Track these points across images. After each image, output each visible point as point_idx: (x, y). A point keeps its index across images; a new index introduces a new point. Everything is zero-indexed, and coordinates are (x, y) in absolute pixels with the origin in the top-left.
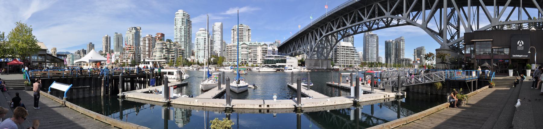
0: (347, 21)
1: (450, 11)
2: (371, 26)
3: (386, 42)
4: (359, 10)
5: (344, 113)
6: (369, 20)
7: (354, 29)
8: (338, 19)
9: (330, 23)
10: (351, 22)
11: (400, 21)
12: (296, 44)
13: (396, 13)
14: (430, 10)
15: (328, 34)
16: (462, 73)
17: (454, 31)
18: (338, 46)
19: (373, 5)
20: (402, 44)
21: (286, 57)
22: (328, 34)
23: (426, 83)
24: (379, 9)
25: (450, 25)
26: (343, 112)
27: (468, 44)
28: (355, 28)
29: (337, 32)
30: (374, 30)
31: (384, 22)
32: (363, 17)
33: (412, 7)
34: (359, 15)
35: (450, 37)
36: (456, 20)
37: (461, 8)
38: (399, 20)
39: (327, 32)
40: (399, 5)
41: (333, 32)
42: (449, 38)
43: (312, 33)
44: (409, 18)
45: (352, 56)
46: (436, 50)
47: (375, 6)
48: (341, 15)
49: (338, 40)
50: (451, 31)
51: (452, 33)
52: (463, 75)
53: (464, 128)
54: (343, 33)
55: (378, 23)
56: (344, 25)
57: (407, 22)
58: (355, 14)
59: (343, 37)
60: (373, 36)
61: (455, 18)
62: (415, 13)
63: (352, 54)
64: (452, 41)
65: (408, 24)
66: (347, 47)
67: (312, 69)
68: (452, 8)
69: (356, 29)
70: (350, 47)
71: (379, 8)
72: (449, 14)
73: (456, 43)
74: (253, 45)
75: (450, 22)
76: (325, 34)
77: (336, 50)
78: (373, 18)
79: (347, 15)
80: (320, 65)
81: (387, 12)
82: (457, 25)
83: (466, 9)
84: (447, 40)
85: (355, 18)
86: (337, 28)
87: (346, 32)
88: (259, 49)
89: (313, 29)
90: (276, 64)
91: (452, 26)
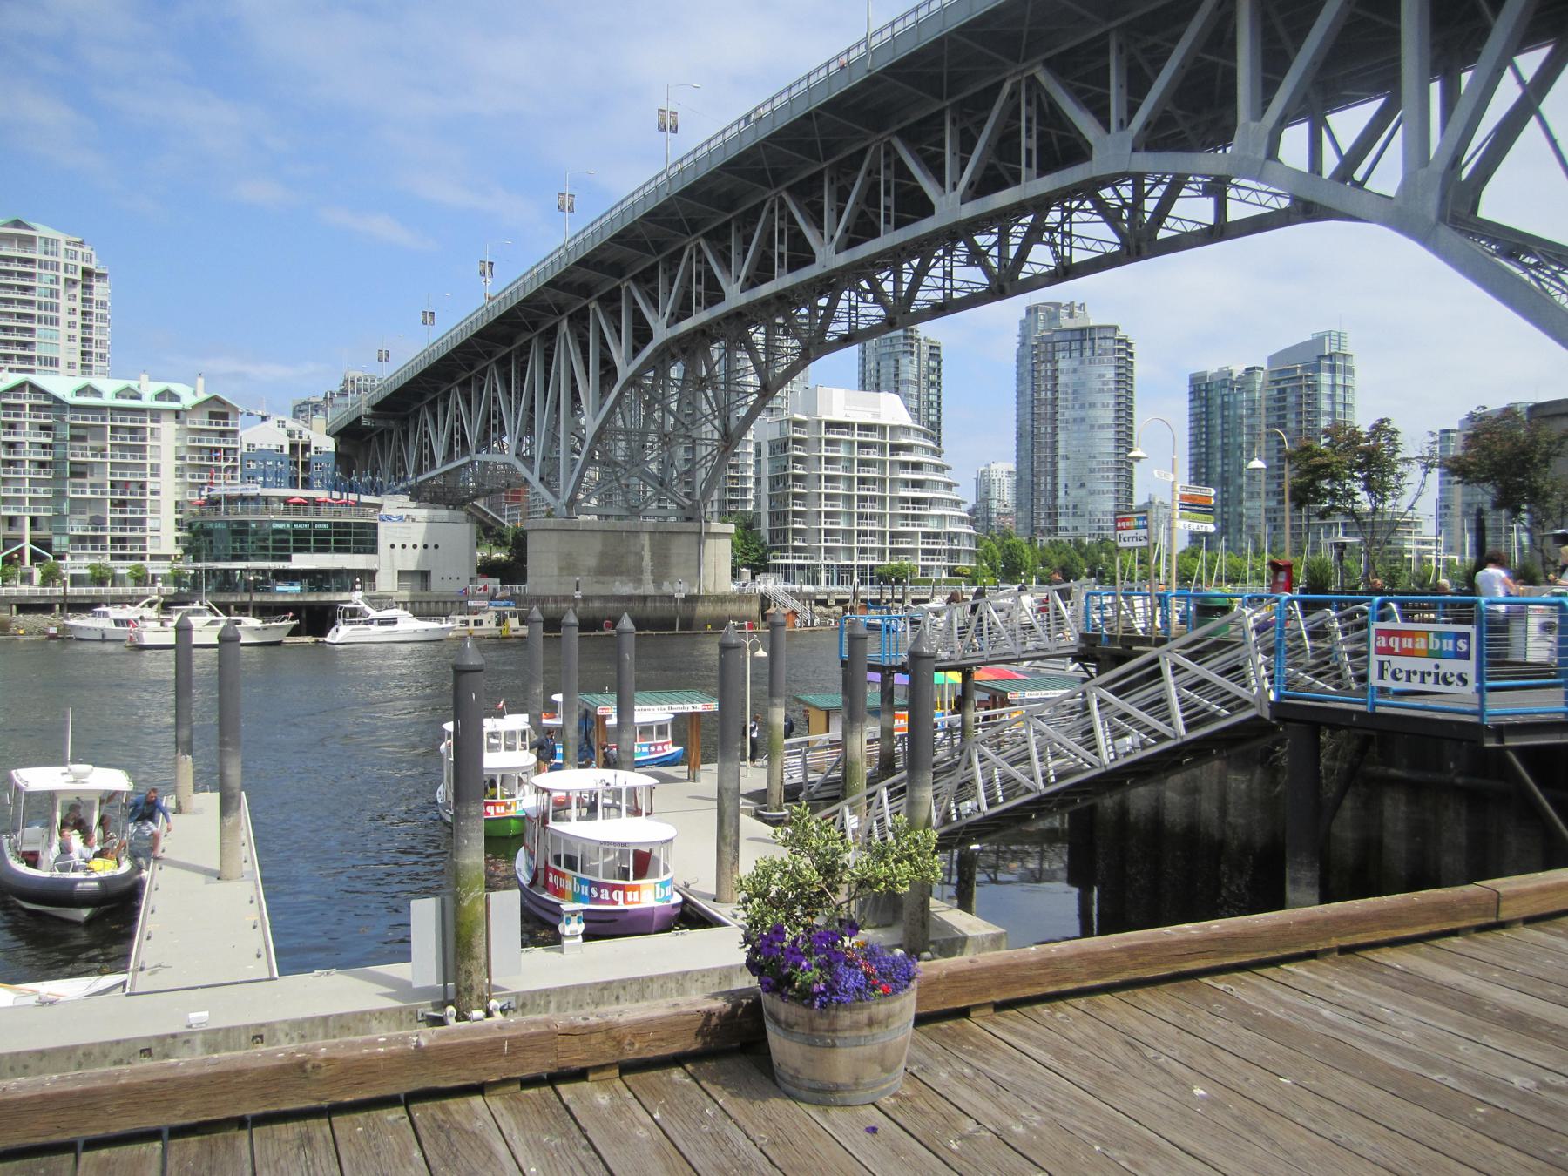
12: (468, 403)
16: (1435, 644)
18: (798, 424)
19: (1000, 85)
20: (1325, 390)
21: (379, 506)
24: (1050, 116)
32: (1085, 123)
34: (902, 171)
38: (1217, 189)
45: (904, 500)
47: (1014, 94)
48: (777, 178)
63: (906, 483)
65: (1305, 210)
67: (578, 595)
70: (893, 428)
74: (108, 400)
81: (1108, 130)
85: (871, 196)
88: (166, 442)
89: (585, 290)
90: (288, 559)
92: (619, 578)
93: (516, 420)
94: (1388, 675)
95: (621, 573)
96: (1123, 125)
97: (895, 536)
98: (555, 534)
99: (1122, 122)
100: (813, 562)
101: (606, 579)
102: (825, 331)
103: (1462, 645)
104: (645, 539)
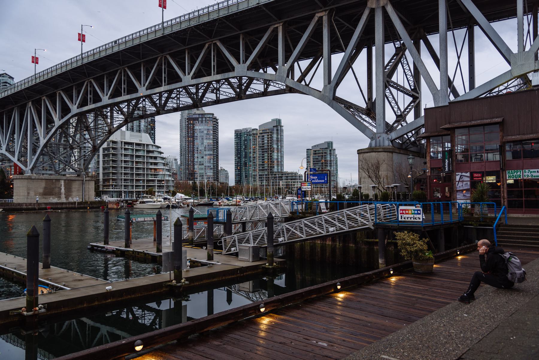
0: (139, 80)
1: (393, 51)
2: (200, 94)
3: (236, 131)
4: (170, 54)
5: (131, 316)
6: (195, 81)
7: (158, 102)
8: (115, 73)
9: (92, 81)
10: (150, 83)
11: (272, 84)
13: (260, 65)
14: (343, 53)
15: (85, 108)
16: (413, 212)
17: (404, 101)
19: (203, 45)
22: (85, 108)
23: (330, 233)
24: (220, 55)
25: (393, 87)
26: (128, 316)
27: (436, 134)
28: (160, 99)
29: (112, 106)
30: (208, 104)
31: (232, 87)
33: (299, 52)
34: (170, 66)
35: (394, 118)
36: (408, 73)
37: (421, 41)
39: (84, 103)
40: (266, 46)
41: (99, 104)
42: (390, 118)
43: (37, 105)
44: (293, 78)
46: (360, 152)
47: (209, 47)
49: (115, 126)
50: (397, 103)
51: (399, 108)
52: (415, 216)
53: (196, 258)
54: (128, 108)
55: (218, 89)
56: (132, 89)
57: (287, 86)
58: (160, 65)
59: (129, 119)
60: (204, 119)
61: (406, 67)
62: (305, 64)
63: (151, 164)
64: (400, 126)
65: (290, 90)
66: (138, 144)
68: (398, 44)
69: (163, 102)
71: (220, 54)
72: (392, 59)
73: (411, 131)
75: (394, 79)
76: (78, 108)
77: (106, 152)
78: (205, 76)
79: (139, 65)
80: (63, 190)
81: (239, 63)
82: (412, 84)
83: (434, 40)
84: (387, 124)
85: (158, 73)
86: (112, 96)
87: (136, 106)
91: (398, 90)
92: (52, 196)
93: (6, 139)
94: (403, 218)
95: (53, 195)
96: (244, 62)
97: (148, 181)
98: (26, 180)
99: (243, 61)
100: (119, 190)
101: (47, 197)
102: (134, 113)
103: (419, 212)
104: (62, 183)
